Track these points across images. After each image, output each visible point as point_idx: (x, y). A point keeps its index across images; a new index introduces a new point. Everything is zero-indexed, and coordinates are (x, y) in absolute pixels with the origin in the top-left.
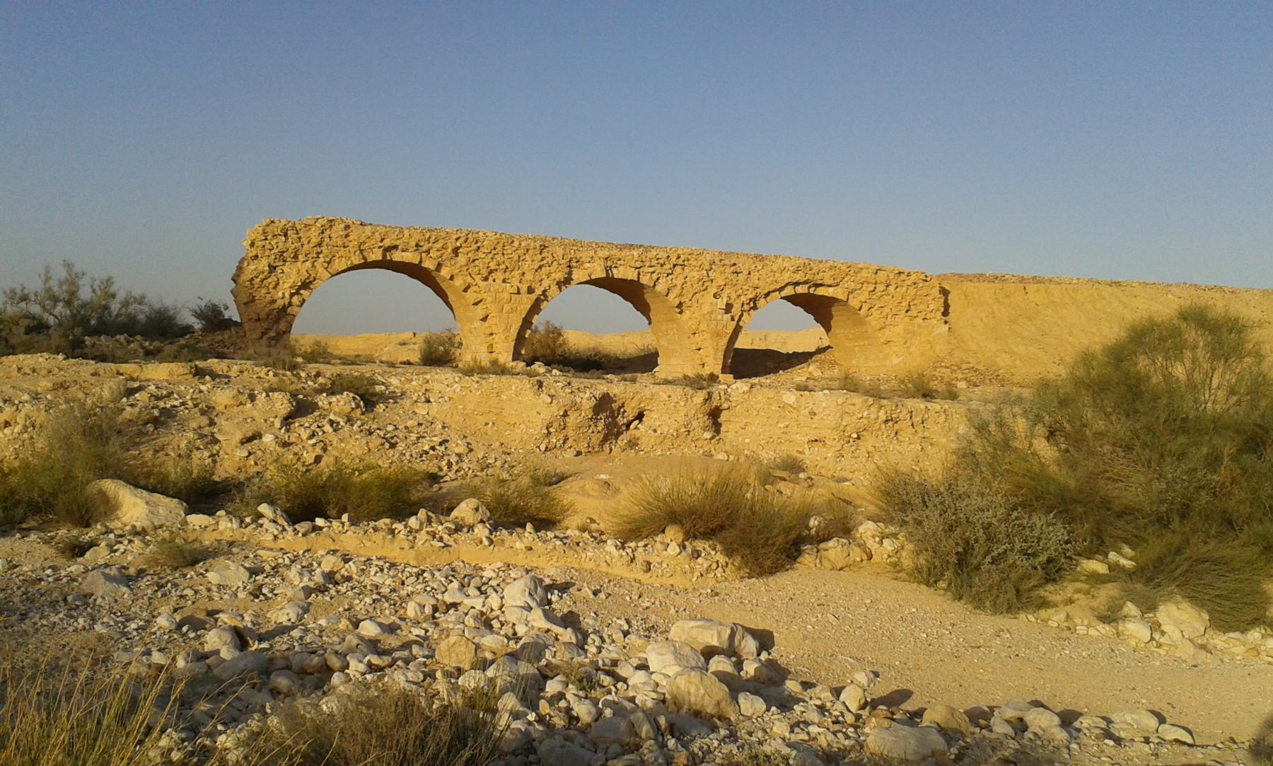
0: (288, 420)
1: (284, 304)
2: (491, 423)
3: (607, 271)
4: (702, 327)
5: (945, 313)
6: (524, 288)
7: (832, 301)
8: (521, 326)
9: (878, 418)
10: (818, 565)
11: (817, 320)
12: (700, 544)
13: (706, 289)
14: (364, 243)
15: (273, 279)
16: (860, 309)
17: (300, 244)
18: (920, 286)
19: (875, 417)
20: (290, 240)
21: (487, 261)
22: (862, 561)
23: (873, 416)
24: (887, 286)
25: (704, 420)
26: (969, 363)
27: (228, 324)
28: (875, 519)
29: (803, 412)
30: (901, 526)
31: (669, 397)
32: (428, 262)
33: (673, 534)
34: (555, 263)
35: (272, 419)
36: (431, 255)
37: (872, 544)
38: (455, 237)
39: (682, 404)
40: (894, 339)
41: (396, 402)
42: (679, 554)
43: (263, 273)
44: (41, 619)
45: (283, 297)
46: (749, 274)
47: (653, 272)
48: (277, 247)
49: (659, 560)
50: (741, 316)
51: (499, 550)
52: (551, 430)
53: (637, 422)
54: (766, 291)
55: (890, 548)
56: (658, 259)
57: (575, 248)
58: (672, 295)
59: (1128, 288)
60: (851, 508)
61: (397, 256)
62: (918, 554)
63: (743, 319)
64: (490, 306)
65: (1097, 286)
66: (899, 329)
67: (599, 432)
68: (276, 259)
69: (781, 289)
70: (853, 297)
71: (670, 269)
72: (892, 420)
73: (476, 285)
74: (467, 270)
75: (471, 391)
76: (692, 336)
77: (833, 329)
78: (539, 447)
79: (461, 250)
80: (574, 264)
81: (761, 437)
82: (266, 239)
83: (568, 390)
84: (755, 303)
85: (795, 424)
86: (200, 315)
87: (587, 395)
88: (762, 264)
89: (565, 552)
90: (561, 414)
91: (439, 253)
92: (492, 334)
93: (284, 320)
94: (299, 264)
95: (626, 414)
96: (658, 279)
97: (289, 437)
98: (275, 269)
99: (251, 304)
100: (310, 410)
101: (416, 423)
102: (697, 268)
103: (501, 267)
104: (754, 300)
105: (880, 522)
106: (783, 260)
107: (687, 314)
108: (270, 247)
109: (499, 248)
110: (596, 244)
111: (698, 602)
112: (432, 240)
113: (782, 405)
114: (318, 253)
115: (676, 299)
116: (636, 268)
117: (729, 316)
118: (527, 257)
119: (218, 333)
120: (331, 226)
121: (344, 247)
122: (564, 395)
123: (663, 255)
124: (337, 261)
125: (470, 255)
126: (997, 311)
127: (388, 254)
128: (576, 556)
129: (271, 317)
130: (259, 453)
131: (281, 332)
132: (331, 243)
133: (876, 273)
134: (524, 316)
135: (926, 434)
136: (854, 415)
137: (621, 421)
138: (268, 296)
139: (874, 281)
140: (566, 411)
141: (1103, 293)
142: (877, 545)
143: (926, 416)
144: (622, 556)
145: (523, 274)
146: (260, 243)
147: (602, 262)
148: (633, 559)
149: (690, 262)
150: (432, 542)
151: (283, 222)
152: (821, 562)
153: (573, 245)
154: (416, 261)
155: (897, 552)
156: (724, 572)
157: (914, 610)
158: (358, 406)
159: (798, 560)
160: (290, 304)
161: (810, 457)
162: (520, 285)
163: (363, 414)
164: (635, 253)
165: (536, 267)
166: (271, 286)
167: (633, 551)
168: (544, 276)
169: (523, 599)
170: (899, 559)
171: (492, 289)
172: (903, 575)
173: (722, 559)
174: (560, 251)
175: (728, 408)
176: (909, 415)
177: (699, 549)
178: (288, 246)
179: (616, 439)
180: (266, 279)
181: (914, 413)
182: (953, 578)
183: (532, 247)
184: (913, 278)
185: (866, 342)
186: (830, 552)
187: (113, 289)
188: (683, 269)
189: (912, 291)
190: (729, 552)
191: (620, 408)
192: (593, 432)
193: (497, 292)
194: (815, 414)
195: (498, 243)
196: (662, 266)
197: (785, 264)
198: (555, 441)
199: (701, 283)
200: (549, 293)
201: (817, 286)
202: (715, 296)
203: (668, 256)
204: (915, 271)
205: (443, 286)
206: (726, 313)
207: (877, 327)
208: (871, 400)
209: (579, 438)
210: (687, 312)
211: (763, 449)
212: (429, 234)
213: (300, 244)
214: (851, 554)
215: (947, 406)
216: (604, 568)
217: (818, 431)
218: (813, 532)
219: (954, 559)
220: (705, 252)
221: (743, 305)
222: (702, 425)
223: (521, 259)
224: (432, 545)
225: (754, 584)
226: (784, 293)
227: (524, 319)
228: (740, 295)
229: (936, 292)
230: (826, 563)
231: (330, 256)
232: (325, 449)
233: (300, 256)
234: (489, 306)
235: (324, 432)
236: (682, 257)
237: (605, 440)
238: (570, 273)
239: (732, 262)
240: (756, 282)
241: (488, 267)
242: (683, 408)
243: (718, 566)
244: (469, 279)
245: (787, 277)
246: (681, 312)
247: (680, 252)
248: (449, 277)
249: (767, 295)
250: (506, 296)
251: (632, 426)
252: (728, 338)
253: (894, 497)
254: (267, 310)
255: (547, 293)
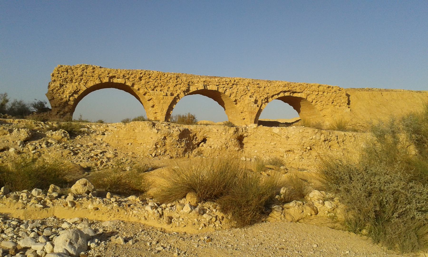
0: (25, 142)
1: (66, 100)
2: (130, 143)
3: (204, 87)
4: (245, 110)
5: (349, 104)
6: (169, 94)
7: (300, 99)
8: (168, 109)
9: (320, 139)
10: (283, 219)
11: (295, 108)
12: (207, 205)
13: (247, 94)
14: (101, 75)
15: (62, 90)
16: (312, 102)
17: (73, 75)
18: (337, 92)
19: (319, 138)
20: (69, 74)
21: (154, 83)
22: (311, 215)
23: (318, 138)
24: (324, 92)
25: (235, 141)
26: (359, 123)
27: (47, 110)
28: (319, 189)
29: (283, 137)
30: (336, 193)
31: (218, 130)
32: (128, 83)
33: (191, 199)
34: (182, 83)
35: (17, 141)
36: (130, 80)
37: (317, 205)
38: (140, 72)
39: (224, 133)
40: (326, 114)
41: (88, 135)
42: (191, 212)
43: (57, 87)
44: (348, 183)
45: (66, 97)
46: (265, 88)
47: (224, 87)
48: (63, 76)
49: (178, 215)
50: (262, 105)
51: (78, 210)
52: (158, 146)
53: (203, 143)
54: (272, 95)
55: (329, 207)
56: (226, 82)
57: (191, 77)
58: (232, 97)
59: (424, 94)
60: (305, 183)
61: (115, 81)
62: (348, 211)
63: (262, 106)
64: (155, 101)
65: (411, 92)
66: (329, 110)
67: (182, 147)
68: (63, 81)
69: (278, 94)
70: (309, 97)
71: (231, 86)
72: (327, 140)
73: (149, 92)
74: (145, 86)
75: (121, 129)
76: (241, 114)
77: (301, 112)
78: (151, 155)
79: (142, 78)
80: (191, 84)
81: (263, 149)
82: (59, 73)
83: (167, 127)
84: (267, 100)
85: (279, 143)
86: (35, 106)
87: (176, 129)
88: (270, 84)
89: (118, 211)
90: (162, 138)
91: (133, 79)
92: (156, 113)
93: (67, 107)
94: (73, 84)
95: (197, 139)
96: (226, 90)
97: (23, 149)
98: (63, 86)
99: (52, 100)
100: (40, 138)
101: (92, 143)
102: (243, 85)
103: (159, 85)
104: (267, 98)
105: (322, 190)
106: (279, 82)
107: (239, 104)
108: (60, 76)
109: (159, 77)
110: (200, 76)
111: (196, 246)
112: (130, 74)
113: (272, 134)
114: (81, 79)
115: (234, 98)
116: (217, 85)
117: (256, 105)
118: (171, 81)
119: (42, 113)
120: (87, 68)
121: (92, 76)
122: (165, 129)
123: (228, 80)
124: (89, 83)
125: (146, 80)
126: (370, 103)
127: (111, 79)
128: (126, 213)
129: (61, 105)
130: (5, 157)
131: (66, 112)
132: (87, 75)
133: (319, 87)
134: (169, 105)
135: (345, 147)
136: (308, 137)
137: (194, 142)
138: (59, 97)
139: (318, 90)
140: (165, 137)
141: (414, 95)
142: (321, 205)
143: (345, 138)
144: (154, 213)
145: (169, 88)
146: (56, 75)
147: (202, 83)
148: (161, 216)
149: (239, 83)
150: (37, 205)
151: (66, 66)
152: (284, 216)
153: (190, 76)
154: (123, 83)
155: (333, 210)
156: (221, 223)
157: (347, 252)
158: (66, 136)
159: (270, 215)
160: (69, 100)
161: (288, 159)
162: (167, 92)
163: (68, 139)
164: (216, 79)
165: (174, 85)
166: (61, 93)
167: (162, 210)
168: (178, 89)
169: (64, 247)
170: (335, 214)
171: (155, 94)
172: (338, 225)
173: (220, 215)
174: (185, 79)
175: (247, 136)
176: (336, 138)
177: (205, 208)
178: (68, 76)
179: (192, 151)
180: (59, 90)
181: (338, 137)
182: (373, 227)
183: (172, 77)
184: (334, 89)
185: (315, 116)
186: (291, 209)
187: (7, 98)
188: (237, 86)
189: (334, 95)
190: (224, 210)
191: (194, 136)
192: (179, 147)
193: (157, 95)
194: (289, 138)
195: (158, 75)
196: (228, 84)
197: (280, 84)
198: (160, 151)
199: (244, 91)
200: (180, 96)
201: (294, 92)
202: (250, 97)
203: (230, 81)
204: (335, 86)
205: (137, 93)
206: (255, 104)
207: (320, 110)
208: (316, 130)
209: (172, 150)
210: (239, 103)
211: (264, 155)
212: (129, 71)
213: (73, 75)
214: (304, 211)
215: (355, 134)
216: (143, 221)
217: (290, 146)
218: (282, 196)
219: (373, 215)
220: (246, 79)
221: (262, 100)
222: (234, 144)
223: (168, 82)
224: (35, 207)
225: (237, 232)
226: (280, 96)
227: (169, 106)
228: (261, 97)
229: (344, 95)
230: (288, 217)
231: (86, 80)
232: (40, 156)
233: (74, 81)
234: (154, 101)
235: (42, 147)
236: (236, 81)
237: (185, 151)
238: (189, 88)
239: (257, 83)
240: (268, 91)
241: (154, 85)
242: (224, 136)
243: (216, 220)
244: (146, 90)
245: (281, 89)
246: (236, 104)
247: (235, 79)
248: (137, 89)
249: (272, 96)
250: (161, 97)
251: (200, 145)
252: (256, 114)
253: (332, 175)
254: (59, 103)
255: (179, 96)
